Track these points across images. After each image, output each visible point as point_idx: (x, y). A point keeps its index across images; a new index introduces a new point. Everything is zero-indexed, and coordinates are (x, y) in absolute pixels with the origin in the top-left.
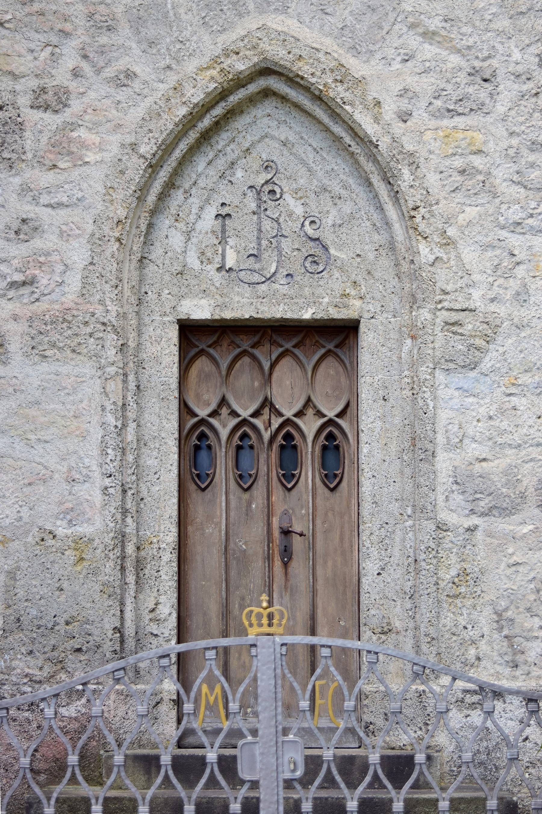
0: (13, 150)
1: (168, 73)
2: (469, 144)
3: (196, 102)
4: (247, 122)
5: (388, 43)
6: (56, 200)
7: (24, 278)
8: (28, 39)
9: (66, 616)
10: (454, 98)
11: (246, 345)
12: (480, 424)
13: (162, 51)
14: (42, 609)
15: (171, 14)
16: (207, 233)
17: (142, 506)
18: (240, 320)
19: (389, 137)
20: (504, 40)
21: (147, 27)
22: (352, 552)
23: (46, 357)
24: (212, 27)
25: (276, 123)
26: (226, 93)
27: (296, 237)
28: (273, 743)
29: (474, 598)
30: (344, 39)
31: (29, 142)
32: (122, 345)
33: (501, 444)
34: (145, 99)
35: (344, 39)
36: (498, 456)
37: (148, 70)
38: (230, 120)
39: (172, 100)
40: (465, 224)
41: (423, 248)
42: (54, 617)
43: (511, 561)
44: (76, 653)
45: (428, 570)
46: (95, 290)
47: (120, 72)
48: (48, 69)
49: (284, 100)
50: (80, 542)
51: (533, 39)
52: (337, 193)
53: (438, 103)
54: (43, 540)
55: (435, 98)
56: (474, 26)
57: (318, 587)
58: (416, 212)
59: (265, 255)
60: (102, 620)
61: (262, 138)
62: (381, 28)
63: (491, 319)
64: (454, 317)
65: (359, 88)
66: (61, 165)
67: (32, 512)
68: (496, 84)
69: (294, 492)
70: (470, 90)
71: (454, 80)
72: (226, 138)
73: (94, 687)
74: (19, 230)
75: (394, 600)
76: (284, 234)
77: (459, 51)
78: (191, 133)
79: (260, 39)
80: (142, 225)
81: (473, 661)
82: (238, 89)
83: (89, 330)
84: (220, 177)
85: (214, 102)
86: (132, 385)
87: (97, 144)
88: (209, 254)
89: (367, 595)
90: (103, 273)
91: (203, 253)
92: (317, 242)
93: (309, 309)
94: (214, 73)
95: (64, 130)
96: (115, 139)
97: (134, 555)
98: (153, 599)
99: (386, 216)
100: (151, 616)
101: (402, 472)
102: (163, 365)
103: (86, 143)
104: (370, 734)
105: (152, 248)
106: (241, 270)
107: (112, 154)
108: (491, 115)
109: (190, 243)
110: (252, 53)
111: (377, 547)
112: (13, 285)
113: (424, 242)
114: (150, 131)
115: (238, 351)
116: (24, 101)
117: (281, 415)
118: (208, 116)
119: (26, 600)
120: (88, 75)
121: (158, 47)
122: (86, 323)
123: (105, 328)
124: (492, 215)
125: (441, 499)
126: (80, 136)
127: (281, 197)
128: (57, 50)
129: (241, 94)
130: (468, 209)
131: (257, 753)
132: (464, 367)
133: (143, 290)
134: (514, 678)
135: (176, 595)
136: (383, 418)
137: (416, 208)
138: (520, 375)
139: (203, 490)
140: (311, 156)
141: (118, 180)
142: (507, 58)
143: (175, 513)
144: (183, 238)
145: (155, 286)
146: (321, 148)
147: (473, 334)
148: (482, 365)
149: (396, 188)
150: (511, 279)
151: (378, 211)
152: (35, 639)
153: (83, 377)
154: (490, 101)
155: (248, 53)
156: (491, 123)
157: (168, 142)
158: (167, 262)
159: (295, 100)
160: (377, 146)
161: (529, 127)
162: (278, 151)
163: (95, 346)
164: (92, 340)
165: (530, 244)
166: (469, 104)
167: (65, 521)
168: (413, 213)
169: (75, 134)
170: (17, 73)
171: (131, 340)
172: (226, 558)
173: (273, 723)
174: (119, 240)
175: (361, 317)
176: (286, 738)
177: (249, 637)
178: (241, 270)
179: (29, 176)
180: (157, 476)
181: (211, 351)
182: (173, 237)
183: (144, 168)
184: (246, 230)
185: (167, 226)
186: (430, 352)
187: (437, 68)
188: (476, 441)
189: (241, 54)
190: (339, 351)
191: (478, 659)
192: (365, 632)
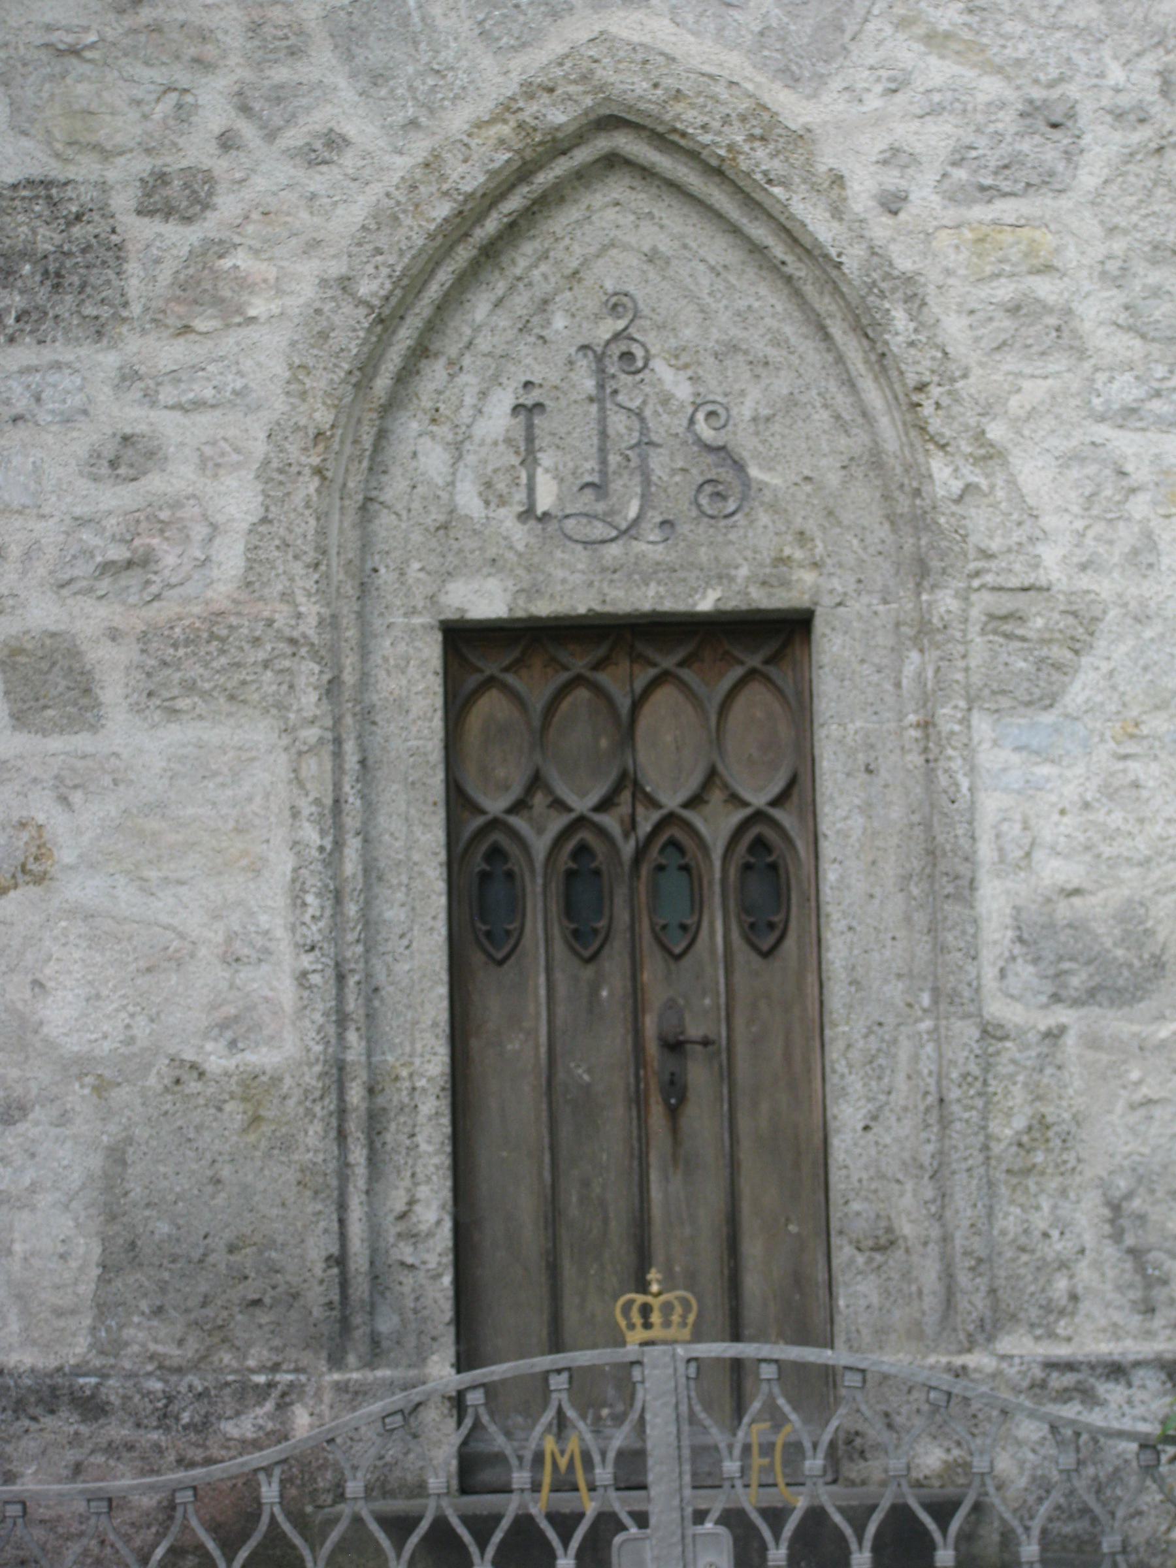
0: (102, 301)
1: (412, 135)
2: (1026, 255)
5: (855, 59)
6: (191, 395)
7: (128, 555)
8: (131, 80)
9: (228, 1235)
10: (993, 164)
11: (580, 664)
12: (1066, 820)
13: (400, 91)
14: (181, 1222)
15: (416, 18)
16: (495, 443)
17: (376, 1003)
18: (567, 617)
19: (864, 246)
20: (1089, 46)
21: (367, 46)
22: (810, 1081)
23: (175, 711)
24: (498, 39)
25: (632, 218)
26: (531, 167)
28: (676, 1538)
29: (1062, 1174)
30: (766, 53)
31: (134, 282)
32: (330, 682)
33: (1109, 858)
34: (367, 189)
35: (766, 53)
36: (1105, 882)
37: (371, 129)
38: (538, 216)
39: (422, 189)
40: (1022, 413)
41: (939, 468)
42: (205, 1237)
43: (1137, 1097)
44: (251, 1309)
45: (967, 1121)
46: (273, 573)
47: (317, 136)
48: (172, 137)
50: (255, 1084)
51: (1147, 43)
53: (961, 174)
54: (178, 1082)
55: (954, 164)
56: (1027, 19)
57: (742, 1156)
58: (923, 396)
59: (616, 485)
60: (302, 1241)
61: (604, 249)
62: (841, 29)
63: (1083, 606)
64: (1007, 603)
66: (200, 325)
67: (154, 1026)
68: (1077, 132)
69: (686, 962)
70: (1025, 146)
71: (991, 128)
73: (290, 1377)
74: (118, 457)
75: (898, 1181)
77: (999, 70)
79: (596, 61)
80: (365, 437)
81: (1064, 1302)
83: (261, 655)
86: (351, 761)
87: (272, 281)
88: (501, 486)
89: (844, 1172)
90: (290, 538)
91: (489, 485)
92: (723, 454)
94: (505, 130)
95: (204, 254)
96: (309, 269)
97: (363, 1106)
98: (402, 1192)
99: (861, 400)
100: (401, 1227)
101: (908, 919)
102: (412, 716)
103: (250, 280)
104: (856, 1456)
105: (384, 478)
106: (567, 516)
107: (301, 301)
108: (1069, 194)
109: (461, 464)
110: (580, 88)
111: (862, 1073)
112: (107, 568)
113: (941, 454)
114: (378, 251)
115: (565, 676)
116: (123, 201)
117: (654, 803)
118: (494, 215)
119: (148, 1205)
120: (251, 145)
121: (391, 83)
122: (256, 642)
123: (294, 649)
124: (1079, 394)
125: (989, 974)
126: (236, 267)
128: (189, 99)
129: (561, 167)
130: (1027, 385)
131: (648, 1556)
132: (1028, 704)
133: (369, 566)
134: (1149, 1334)
135: (449, 1183)
136: (867, 808)
137: (921, 388)
138: (1144, 717)
139: (500, 963)
140: (705, 281)
141: (315, 352)
142: (1095, 81)
143: (443, 1017)
144: (446, 456)
145: (393, 555)
146: (725, 267)
147: (1047, 636)
148: (1067, 699)
149: (880, 348)
150: (1121, 524)
151: (844, 389)
152: (166, 1282)
153: (251, 749)
154: (1066, 168)
155: (572, 89)
156: (1070, 211)
157: (414, 271)
158: (416, 505)
159: (669, 175)
160: (838, 266)
161: (1148, 215)
163: (274, 687)
164: (269, 674)
165: (1157, 451)
166: (1024, 175)
167: (223, 1043)
168: (915, 398)
169: (226, 263)
170: (109, 148)
171: (348, 669)
172: (550, 1104)
173: (676, 1502)
174: (318, 471)
176: (699, 1529)
177: (629, 1347)
178: (567, 516)
179: (135, 350)
180: (405, 942)
181: (510, 679)
183: (366, 325)
184: (575, 435)
185: (414, 434)
186: (959, 676)
187: (957, 105)
188: (1059, 854)
189: (559, 91)
190: (772, 670)
191: (1074, 1297)
192: (841, 1248)
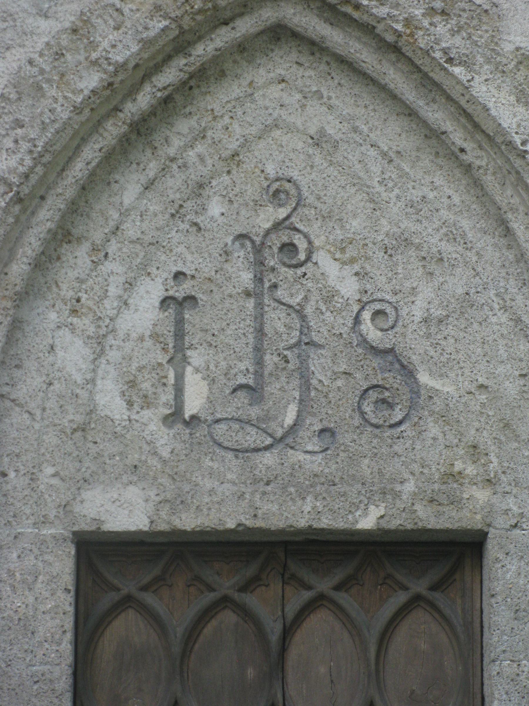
3: (120, 59)
4: (234, 95)
16: (142, 339)
25: (298, 96)
26: (189, 37)
27: (341, 348)
34: (8, 54)
38: (196, 91)
39: (69, 57)
49: (315, 49)
52: (434, 250)
61: (267, 129)
65: (484, 27)
72: (185, 131)
76: (316, 339)
78: (109, 125)
82: (215, 27)
84: (173, 215)
85: (160, 58)
88: (146, 386)
91: (132, 384)
92: (390, 358)
93: (372, 508)
102: (38, 638)
105: (17, 373)
106: (218, 421)
115: (210, 597)
118: (147, 88)
127: (308, 258)
144: (87, 351)
145: (24, 458)
146: (398, 152)
157: (57, 147)
158: (52, 404)
159: (339, 51)
162: (302, 157)
175: (489, 525)
178: (218, 421)
182: (65, 349)
184: (229, 332)
185: (52, 326)
190: (437, 597)
